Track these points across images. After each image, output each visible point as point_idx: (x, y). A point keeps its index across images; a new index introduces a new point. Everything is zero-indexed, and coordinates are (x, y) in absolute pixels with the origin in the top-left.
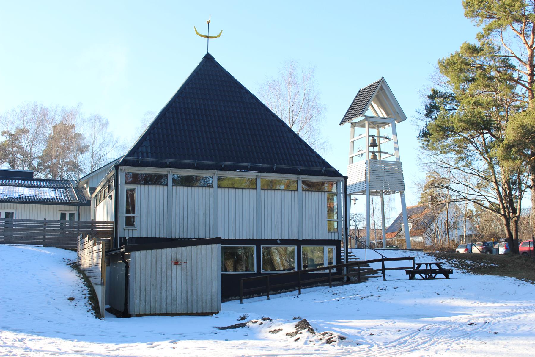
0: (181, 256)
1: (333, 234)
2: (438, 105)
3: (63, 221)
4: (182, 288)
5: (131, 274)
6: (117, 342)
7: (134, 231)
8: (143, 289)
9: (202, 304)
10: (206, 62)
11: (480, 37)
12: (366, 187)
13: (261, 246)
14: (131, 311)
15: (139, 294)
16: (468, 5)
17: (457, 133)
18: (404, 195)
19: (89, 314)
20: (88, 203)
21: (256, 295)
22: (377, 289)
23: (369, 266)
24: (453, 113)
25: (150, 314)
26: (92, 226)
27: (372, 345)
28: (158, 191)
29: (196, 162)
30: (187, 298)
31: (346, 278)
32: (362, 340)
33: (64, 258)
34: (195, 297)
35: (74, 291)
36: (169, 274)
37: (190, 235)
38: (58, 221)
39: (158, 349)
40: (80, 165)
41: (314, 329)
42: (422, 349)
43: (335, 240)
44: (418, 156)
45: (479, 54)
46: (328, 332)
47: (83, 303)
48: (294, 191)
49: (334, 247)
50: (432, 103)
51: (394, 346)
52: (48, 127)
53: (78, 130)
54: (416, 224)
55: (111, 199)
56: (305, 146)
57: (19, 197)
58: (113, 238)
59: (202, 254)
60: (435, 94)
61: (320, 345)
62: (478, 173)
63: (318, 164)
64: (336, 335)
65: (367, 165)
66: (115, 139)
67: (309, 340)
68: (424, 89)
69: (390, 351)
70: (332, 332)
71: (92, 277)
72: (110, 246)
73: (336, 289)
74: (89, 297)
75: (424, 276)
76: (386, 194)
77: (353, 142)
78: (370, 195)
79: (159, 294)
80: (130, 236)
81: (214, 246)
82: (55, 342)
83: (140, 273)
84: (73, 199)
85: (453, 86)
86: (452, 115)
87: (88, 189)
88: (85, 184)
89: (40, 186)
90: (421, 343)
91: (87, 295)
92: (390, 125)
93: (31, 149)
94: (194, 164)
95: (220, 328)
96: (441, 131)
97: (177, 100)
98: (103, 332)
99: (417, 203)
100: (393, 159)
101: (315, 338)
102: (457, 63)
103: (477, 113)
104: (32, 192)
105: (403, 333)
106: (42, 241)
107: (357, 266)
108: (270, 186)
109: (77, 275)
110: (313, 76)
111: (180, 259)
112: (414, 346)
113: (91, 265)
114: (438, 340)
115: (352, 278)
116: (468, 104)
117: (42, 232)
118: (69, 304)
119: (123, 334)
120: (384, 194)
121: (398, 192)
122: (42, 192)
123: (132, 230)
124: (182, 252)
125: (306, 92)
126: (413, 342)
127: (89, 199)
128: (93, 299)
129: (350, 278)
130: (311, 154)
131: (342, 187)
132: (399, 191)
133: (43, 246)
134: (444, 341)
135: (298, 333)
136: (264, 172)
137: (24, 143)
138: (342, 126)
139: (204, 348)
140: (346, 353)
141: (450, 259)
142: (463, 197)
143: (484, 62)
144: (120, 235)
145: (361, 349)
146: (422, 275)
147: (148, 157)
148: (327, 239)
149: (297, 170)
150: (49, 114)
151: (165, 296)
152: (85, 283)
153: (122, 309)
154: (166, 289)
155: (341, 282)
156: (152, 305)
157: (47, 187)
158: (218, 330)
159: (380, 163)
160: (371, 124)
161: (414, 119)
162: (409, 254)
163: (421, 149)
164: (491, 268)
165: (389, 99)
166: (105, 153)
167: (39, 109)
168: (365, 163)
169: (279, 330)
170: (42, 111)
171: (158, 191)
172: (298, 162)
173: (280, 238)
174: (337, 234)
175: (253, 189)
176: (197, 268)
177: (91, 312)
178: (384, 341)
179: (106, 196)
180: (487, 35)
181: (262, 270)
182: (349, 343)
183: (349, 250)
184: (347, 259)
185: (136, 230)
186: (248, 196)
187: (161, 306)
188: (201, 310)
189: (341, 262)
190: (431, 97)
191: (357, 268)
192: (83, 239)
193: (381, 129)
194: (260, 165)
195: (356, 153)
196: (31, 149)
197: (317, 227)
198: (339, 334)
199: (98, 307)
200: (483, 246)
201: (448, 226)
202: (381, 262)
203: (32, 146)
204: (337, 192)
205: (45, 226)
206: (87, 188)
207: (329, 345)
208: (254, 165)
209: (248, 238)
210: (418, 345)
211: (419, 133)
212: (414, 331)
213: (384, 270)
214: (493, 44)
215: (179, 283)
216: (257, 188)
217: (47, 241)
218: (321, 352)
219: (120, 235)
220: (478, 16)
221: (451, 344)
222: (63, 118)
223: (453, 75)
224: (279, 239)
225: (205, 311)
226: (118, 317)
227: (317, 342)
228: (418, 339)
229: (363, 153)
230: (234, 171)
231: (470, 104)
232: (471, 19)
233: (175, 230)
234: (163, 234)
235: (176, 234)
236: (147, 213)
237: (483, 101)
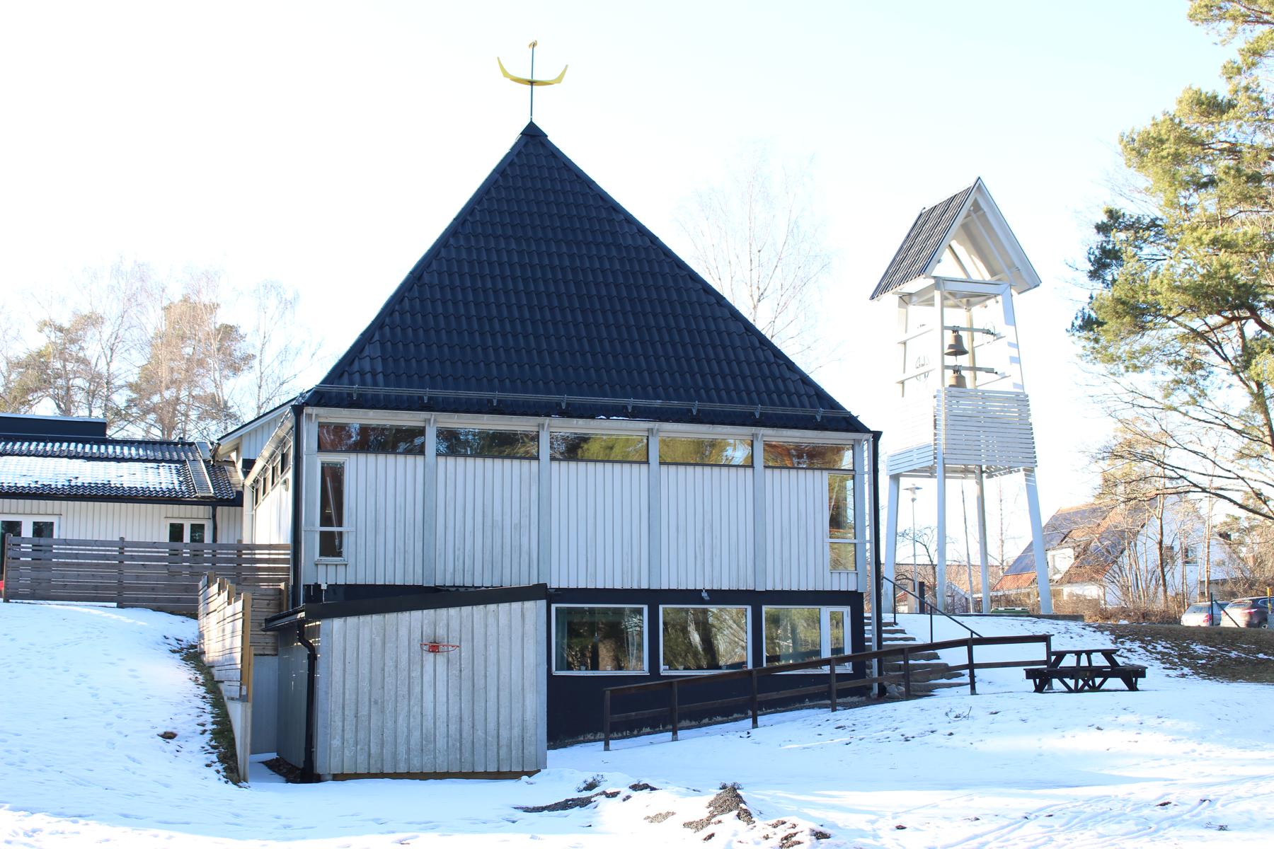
0: (445, 630)
1: (844, 576)
2: (1120, 249)
4: (448, 711)
5: (320, 674)
7: (341, 569)
8: (349, 713)
10: (526, 145)
11: (1232, 71)
12: (935, 458)
14: (320, 768)
15: (340, 724)
17: (1169, 319)
20: (237, 501)
21: (648, 730)
22: (947, 714)
23: (938, 658)
24: (1158, 268)
26: (239, 556)
29: (496, 396)
31: (876, 686)
33: (167, 636)
34: (480, 733)
37: (482, 579)
41: (751, 812)
45: (1225, 117)
47: (197, 746)
48: (743, 469)
49: (846, 610)
50: (1104, 244)
54: (1083, 553)
56: (774, 355)
57: (67, 483)
58: (287, 586)
60: (1112, 221)
62: (1225, 420)
63: (805, 399)
65: (938, 401)
71: (222, 682)
72: (280, 605)
73: (844, 716)
75: (1071, 683)
76: (990, 476)
78: (945, 477)
79: (390, 724)
81: (529, 605)
83: (344, 671)
84: (201, 489)
85: (1161, 199)
86: (1156, 274)
87: (239, 465)
88: (233, 450)
89: (121, 456)
91: (209, 727)
92: (999, 298)
93: (108, 364)
94: (490, 401)
95: (527, 810)
96: (1128, 313)
97: (452, 241)
98: (237, 815)
100: (1005, 386)
102: (1167, 140)
103: (1218, 267)
105: (983, 824)
106: (114, 594)
107: (902, 656)
108: (703, 456)
111: (444, 639)
114: (1067, 842)
115: (893, 689)
116: (1197, 244)
117: (115, 572)
118: (161, 747)
120: (984, 475)
121: (1019, 471)
123: (336, 565)
124: (448, 620)
127: (240, 489)
128: (222, 735)
129: (888, 688)
130: (788, 374)
132: (1021, 469)
133: (118, 607)
135: (713, 820)
136: (667, 420)
137: (92, 348)
141: (1150, 642)
142: (1188, 483)
143: (1237, 136)
144: (306, 578)
146: (1065, 680)
147: (375, 384)
148: (828, 588)
152: (208, 696)
153: (299, 760)
155: (864, 698)
156: (372, 751)
157: (139, 460)
158: (521, 814)
160: (949, 296)
162: (1041, 628)
163: (1078, 360)
164: (1256, 664)
165: (996, 235)
168: (935, 397)
172: (754, 395)
173: (708, 587)
175: (640, 463)
176: (486, 661)
177: (216, 768)
180: (1249, 68)
181: (662, 667)
183: (887, 617)
184: (880, 639)
185: (346, 565)
187: (395, 755)
188: (496, 766)
189: (864, 648)
190: (1102, 228)
191: (902, 662)
192: (209, 587)
193: (976, 310)
194: (657, 403)
195: (911, 370)
197: (803, 560)
199: (234, 755)
200: (1252, 607)
201: (1166, 555)
204: (854, 470)
205: (121, 557)
208: (642, 403)
213: (971, 666)
214: (1260, 89)
215: (442, 698)
217: (127, 594)
219: (306, 578)
220: (1221, 18)
223: (1158, 173)
225: (505, 769)
226: (288, 781)
229: (928, 372)
230: (593, 417)
231: (1201, 244)
232: (1205, 25)
233: (443, 567)
234: (413, 577)
235: (444, 577)
236: (374, 524)
237: (1235, 237)
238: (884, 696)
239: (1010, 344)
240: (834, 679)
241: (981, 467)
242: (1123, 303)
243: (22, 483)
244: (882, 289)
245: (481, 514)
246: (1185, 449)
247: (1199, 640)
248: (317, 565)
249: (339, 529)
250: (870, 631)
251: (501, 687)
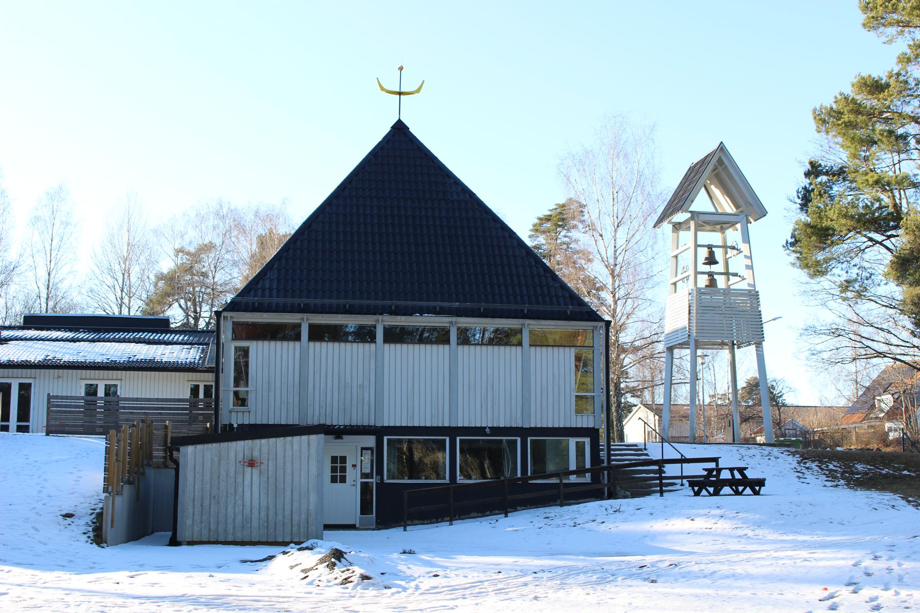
1: (585, 418)
7: (246, 414)
10: (393, 136)
14: (179, 539)
16: (866, 8)
18: (762, 348)
25: (209, 541)
28: (285, 351)
30: (268, 518)
34: (280, 517)
36: (239, 480)
38: (82, 398)
43: (588, 428)
49: (587, 441)
58: (210, 425)
59: (292, 450)
65: (692, 296)
76: (739, 348)
77: (676, 257)
79: (223, 511)
83: (195, 478)
92: (738, 226)
100: (743, 286)
110: (653, 140)
120: (736, 346)
124: (260, 447)
136: (461, 316)
148: (574, 426)
151: (232, 514)
154: (235, 504)
156: (212, 528)
165: (735, 181)
168: (690, 294)
171: (285, 351)
176: (284, 473)
181: (458, 478)
182: (373, 585)
184: (609, 460)
186: (428, 356)
187: (226, 530)
188: (290, 538)
209: (435, 425)
230: (411, 315)
234: (292, 419)
238: (612, 496)
239: (746, 257)
240: (562, 487)
241: (733, 342)
242: (812, 227)
243: (99, 360)
244: (660, 220)
245: (337, 378)
246: (872, 326)
247: (863, 462)
248: (231, 412)
249: (246, 389)
250: (603, 454)
251: (294, 489)
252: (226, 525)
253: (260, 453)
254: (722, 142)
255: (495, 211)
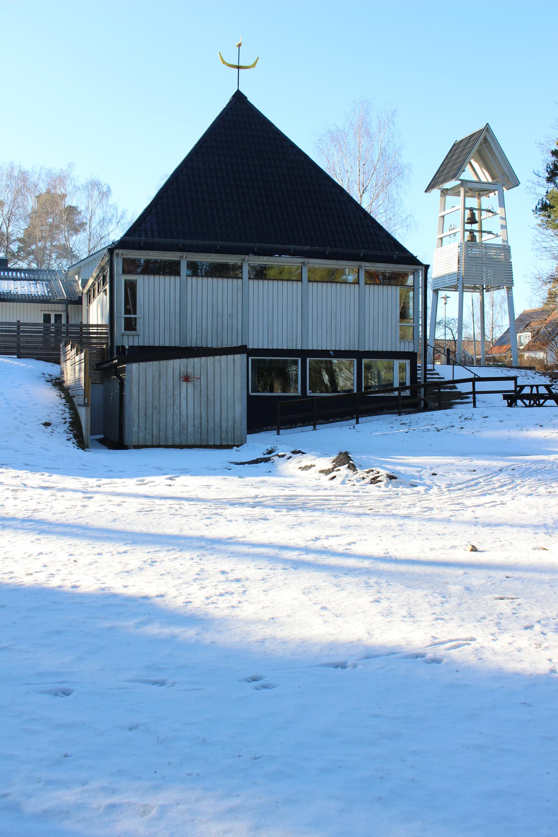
1: (407, 344)
3: (48, 325)
4: (194, 413)
5: (126, 393)
6: (100, 476)
7: (136, 338)
8: (142, 413)
9: (221, 434)
12: (458, 280)
13: (308, 359)
14: (127, 441)
15: (137, 419)
19: (70, 443)
20: (79, 302)
22: (460, 417)
27: (430, 487)
30: (201, 425)
31: (422, 402)
32: (418, 481)
34: (211, 424)
35: (51, 415)
36: (177, 393)
39: (150, 486)
40: (73, 250)
42: (496, 494)
44: (533, 238)
46: (374, 469)
49: (408, 362)
51: (460, 489)
52: (29, 197)
53: (69, 202)
54: (536, 335)
55: (106, 295)
58: (107, 346)
61: (362, 485)
64: (383, 472)
65: (460, 249)
66: (120, 214)
67: (348, 479)
68: (548, 142)
69: (453, 495)
70: (379, 469)
73: (405, 418)
74: (70, 422)
75: (527, 402)
76: (488, 291)
78: (463, 291)
79: (163, 419)
80: (131, 344)
81: (237, 356)
82: (21, 476)
84: (60, 295)
87: (80, 282)
88: (76, 275)
90: (497, 486)
91: (68, 420)
92: (496, 192)
93: (7, 228)
94: (216, 246)
95: (237, 464)
98: (84, 465)
99: (543, 305)
100: (498, 241)
101: (356, 476)
104: (6, 285)
105: (478, 473)
106: (15, 351)
109: (58, 394)
110: (393, 123)
112: (486, 489)
113: (73, 382)
114: (522, 483)
115: (432, 404)
117: (15, 339)
118: (43, 430)
119: (110, 469)
120: (485, 290)
121: (504, 288)
122: (19, 286)
123: (133, 335)
124: (194, 364)
125: (383, 146)
126: (488, 485)
127: (80, 295)
129: (429, 404)
131: (420, 279)
132: (505, 287)
133: (18, 358)
134: (529, 485)
135: (335, 469)
136: (312, 257)
138: (428, 194)
139: (209, 486)
140: (393, 496)
144: (117, 343)
145: (415, 492)
147: (153, 236)
148: (398, 350)
149: (359, 255)
150: (31, 179)
152: (67, 404)
154: (173, 413)
156: (154, 434)
158: (233, 465)
159: (479, 246)
161: (530, 185)
166: (107, 233)
167: (16, 173)
168: (459, 247)
169: (312, 466)
170: (21, 174)
173: (333, 349)
174: (412, 343)
176: (214, 387)
177: (72, 441)
178: (448, 482)
179: (100, 291)
181: (308, 391)
183: (429, 366)
184: (425, 378)
185: (138, 335)
186: (324, 291)
187: (166, 435)
192: (66, 347)
193: (483, 199)
195: (446, 233)
196: (7, 228)
198: (387, 472)
202: (471, 383)
203: (9, 224)
204: (414, 286)
205: (18, 331)
206: (79, 280)
207: (373, 485)
208: (299, 248)
209: (290, 348)
210: (492, 489)
211: (537, 204)
212: (493, 472)
213: (474, 393)
215: (191, 406)
216: (303, 280)
217: (22, 351)
218: (360, 494)
219: (117, 343)
221: (537, 488)
222: (49, 184)
224: (333, 349)
227: (358, 481)
228: (495, 482)
229: (456, 233)
230: (272, 255)
233: (190, 337)
234: (175, 342)
235: (192, 341)
238: (427, 408)
239: (501, 218)
252: (167, 431)
253: (194, 370)
254: (488, 124)
255: (162, 183)
